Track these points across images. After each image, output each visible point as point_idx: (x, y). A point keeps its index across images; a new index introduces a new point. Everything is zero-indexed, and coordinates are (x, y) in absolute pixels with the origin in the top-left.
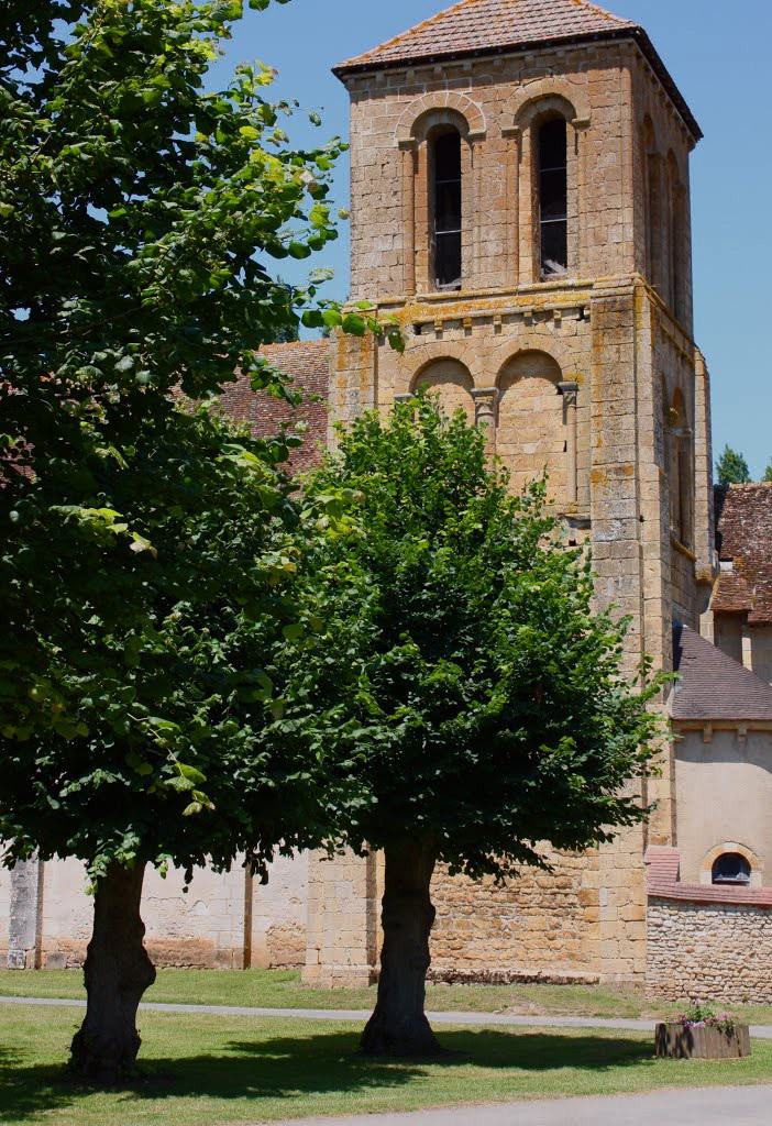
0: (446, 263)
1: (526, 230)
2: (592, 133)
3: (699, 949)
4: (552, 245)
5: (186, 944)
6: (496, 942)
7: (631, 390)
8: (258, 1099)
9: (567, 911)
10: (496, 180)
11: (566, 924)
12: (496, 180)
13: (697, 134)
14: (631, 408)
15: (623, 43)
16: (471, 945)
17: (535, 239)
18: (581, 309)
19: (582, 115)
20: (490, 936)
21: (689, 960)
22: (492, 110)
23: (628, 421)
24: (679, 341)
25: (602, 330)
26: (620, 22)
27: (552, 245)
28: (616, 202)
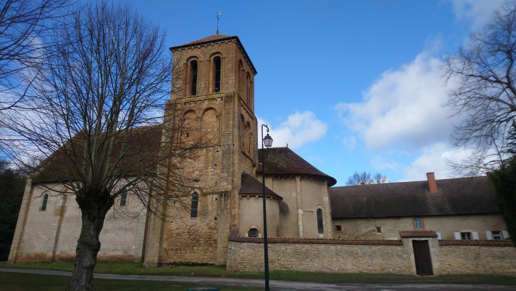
0: (194, 92)
1: (211, 82)
2: (226, 60)
3: (241, 255)
4: (217, 87)
5: (129, 256)
6: (192, 254)
7: (232, 115)
8: (377, 220)
9: (210, 245)
10: (205, 72)
11: (210, 249)
12: (205, 72)
13: (256, 73)
14: (232, 119)
15: (233, 40)
16: (186, 255)
17: (213, 84)
18: (222, 98)
19: (224, 56)
20: (191, 252)
21: (238, 259)
22: (203, 55)
23: (231, 122)
24: (252, 115)
25: (226, 102)
26: (232, 35)
27: (217, 87)
28: (231, 75)
